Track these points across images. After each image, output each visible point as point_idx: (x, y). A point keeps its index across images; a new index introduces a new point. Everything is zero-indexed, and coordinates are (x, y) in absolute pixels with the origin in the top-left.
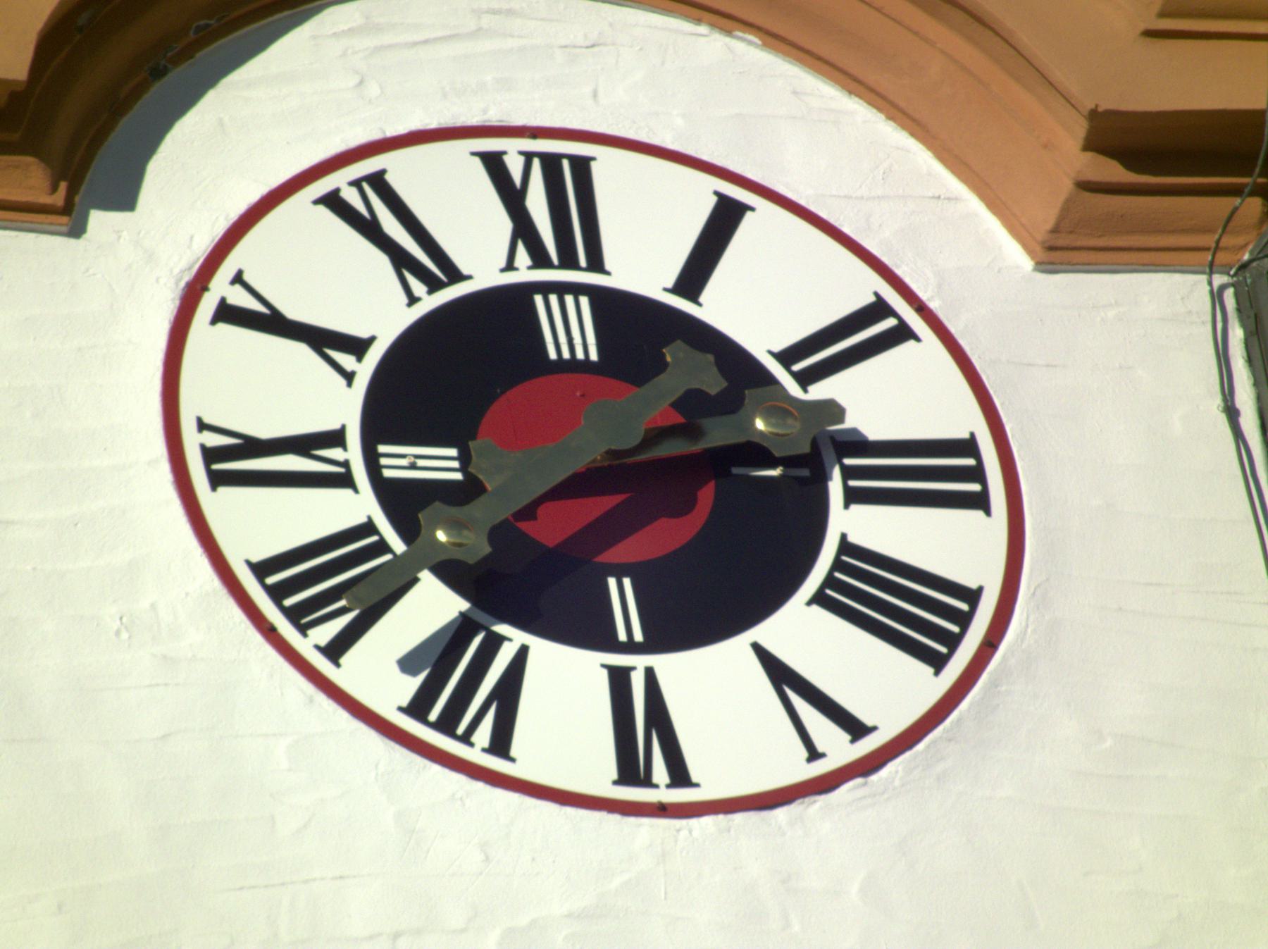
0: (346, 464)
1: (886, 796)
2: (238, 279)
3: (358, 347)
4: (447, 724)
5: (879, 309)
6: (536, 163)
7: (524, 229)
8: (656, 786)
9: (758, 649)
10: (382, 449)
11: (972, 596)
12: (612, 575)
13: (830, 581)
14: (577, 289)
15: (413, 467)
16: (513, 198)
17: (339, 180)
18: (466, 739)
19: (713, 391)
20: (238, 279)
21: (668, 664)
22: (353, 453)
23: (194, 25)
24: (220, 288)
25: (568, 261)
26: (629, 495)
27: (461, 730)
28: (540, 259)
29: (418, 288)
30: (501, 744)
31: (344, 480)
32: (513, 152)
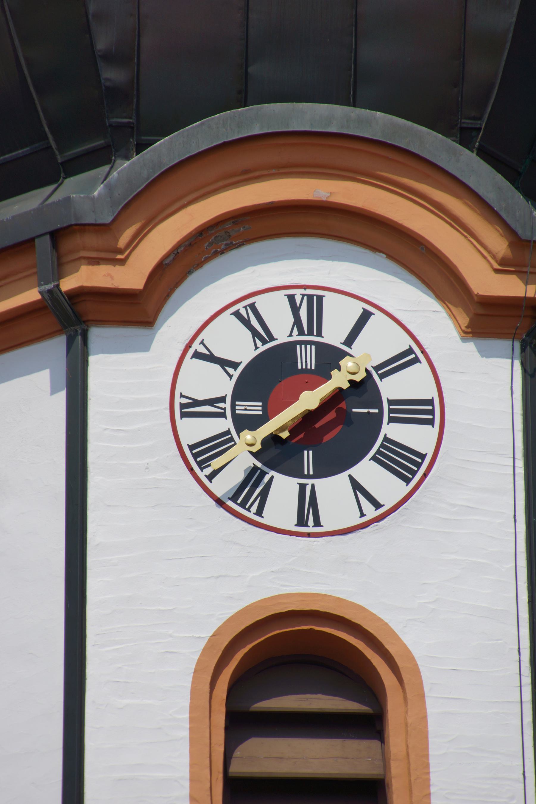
0: (224, 409)
1: (383, 529)
2: (202, 343)
3: (235, 365)
4: (243, 505)
5: (410, 351)
6: (306, 297)
7: (297, 322)
8: (309, 527)
9: (350, 477)
10: (237, 403)
11: (423, 457)
12: (313, 370)
13: (378, 452)
14: (311, 343)
15: (246, 410)
16: (295, 310)
17: (240, 306)
18: (248, 510)
19: (345, 388)
20: (202, 343)
21: (319, 483)
22: (227, 405)
23: (204, 257)
24: (197, 346)
25: (310, 333)
26: (304, 433)
27: (247, 507)
28: (301, 332)
29: (259, 343)
30: (259, 512)
31: (223, 415)
32: (298, 293)
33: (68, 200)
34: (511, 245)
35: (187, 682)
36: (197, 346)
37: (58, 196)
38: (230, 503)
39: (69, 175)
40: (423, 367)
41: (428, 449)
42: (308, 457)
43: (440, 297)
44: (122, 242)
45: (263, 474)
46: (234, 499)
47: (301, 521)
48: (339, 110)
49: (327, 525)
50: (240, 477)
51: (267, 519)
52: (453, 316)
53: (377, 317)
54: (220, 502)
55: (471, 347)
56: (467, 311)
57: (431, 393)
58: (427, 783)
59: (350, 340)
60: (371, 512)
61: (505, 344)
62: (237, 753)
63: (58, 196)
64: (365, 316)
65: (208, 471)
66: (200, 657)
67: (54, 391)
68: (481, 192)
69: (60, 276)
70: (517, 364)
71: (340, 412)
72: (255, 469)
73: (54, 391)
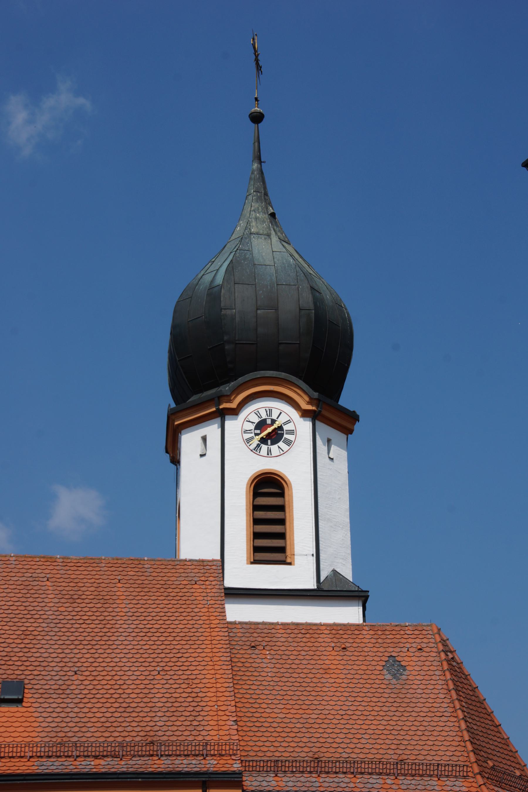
3: (254, 423)
4: (256, 451)
7: (267, 414)
16: (267, 412)
22: (253, 431)
24: (247, 419)
28: (268, 416)
31: (252, 433)
32: (267, 409)
33: (221, 390)
34: (310, 399)
35: (245, 487)
36: (247, 419)
37: (219, 389)
38: (254, 451)
39: (221, 385)
40: (292, 423)
41: (293, 440)
42: (269, 441)
43: (296, 409)
44: (232, 398)
45: (260, 445)
46: (254, 450)
47: (268, 454)
48: (275, 372)
49: (273, 455)
50: (256, 446)
51: (261, 454)
52: (298, 413)
53: (283, 414)
54: (252, 451)
55: (302, 419)
56: (301, 412)
57: (294, 429)
58: (293, 506)
59: (277, 418)
60: (282, 452)
61: (308, 419)
62: (255, 500)
63: (219, 389)
64: (281, 413)
65: (249, 444)
66: (301, 380)
67: (218, 428)
68: (303, 388)
69: (219, 405)
70: (311, 423)
71: (276, 432)
72: (258, 444)
73: (218, 428)
